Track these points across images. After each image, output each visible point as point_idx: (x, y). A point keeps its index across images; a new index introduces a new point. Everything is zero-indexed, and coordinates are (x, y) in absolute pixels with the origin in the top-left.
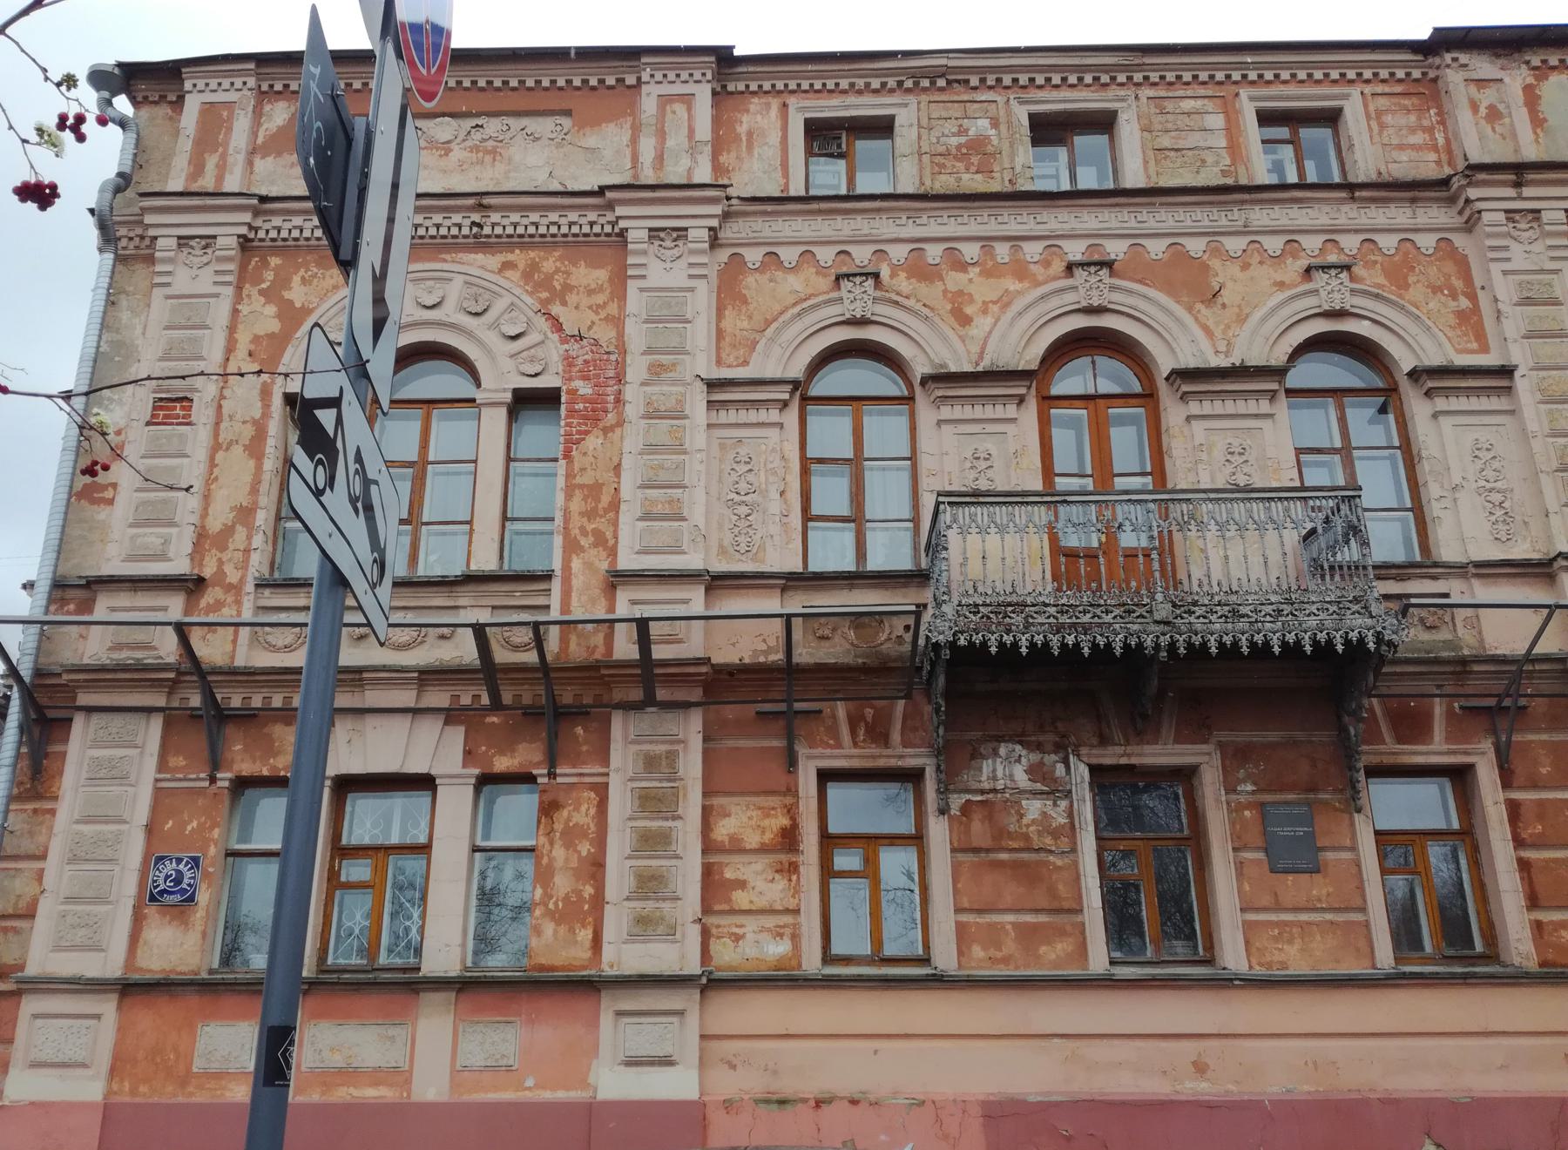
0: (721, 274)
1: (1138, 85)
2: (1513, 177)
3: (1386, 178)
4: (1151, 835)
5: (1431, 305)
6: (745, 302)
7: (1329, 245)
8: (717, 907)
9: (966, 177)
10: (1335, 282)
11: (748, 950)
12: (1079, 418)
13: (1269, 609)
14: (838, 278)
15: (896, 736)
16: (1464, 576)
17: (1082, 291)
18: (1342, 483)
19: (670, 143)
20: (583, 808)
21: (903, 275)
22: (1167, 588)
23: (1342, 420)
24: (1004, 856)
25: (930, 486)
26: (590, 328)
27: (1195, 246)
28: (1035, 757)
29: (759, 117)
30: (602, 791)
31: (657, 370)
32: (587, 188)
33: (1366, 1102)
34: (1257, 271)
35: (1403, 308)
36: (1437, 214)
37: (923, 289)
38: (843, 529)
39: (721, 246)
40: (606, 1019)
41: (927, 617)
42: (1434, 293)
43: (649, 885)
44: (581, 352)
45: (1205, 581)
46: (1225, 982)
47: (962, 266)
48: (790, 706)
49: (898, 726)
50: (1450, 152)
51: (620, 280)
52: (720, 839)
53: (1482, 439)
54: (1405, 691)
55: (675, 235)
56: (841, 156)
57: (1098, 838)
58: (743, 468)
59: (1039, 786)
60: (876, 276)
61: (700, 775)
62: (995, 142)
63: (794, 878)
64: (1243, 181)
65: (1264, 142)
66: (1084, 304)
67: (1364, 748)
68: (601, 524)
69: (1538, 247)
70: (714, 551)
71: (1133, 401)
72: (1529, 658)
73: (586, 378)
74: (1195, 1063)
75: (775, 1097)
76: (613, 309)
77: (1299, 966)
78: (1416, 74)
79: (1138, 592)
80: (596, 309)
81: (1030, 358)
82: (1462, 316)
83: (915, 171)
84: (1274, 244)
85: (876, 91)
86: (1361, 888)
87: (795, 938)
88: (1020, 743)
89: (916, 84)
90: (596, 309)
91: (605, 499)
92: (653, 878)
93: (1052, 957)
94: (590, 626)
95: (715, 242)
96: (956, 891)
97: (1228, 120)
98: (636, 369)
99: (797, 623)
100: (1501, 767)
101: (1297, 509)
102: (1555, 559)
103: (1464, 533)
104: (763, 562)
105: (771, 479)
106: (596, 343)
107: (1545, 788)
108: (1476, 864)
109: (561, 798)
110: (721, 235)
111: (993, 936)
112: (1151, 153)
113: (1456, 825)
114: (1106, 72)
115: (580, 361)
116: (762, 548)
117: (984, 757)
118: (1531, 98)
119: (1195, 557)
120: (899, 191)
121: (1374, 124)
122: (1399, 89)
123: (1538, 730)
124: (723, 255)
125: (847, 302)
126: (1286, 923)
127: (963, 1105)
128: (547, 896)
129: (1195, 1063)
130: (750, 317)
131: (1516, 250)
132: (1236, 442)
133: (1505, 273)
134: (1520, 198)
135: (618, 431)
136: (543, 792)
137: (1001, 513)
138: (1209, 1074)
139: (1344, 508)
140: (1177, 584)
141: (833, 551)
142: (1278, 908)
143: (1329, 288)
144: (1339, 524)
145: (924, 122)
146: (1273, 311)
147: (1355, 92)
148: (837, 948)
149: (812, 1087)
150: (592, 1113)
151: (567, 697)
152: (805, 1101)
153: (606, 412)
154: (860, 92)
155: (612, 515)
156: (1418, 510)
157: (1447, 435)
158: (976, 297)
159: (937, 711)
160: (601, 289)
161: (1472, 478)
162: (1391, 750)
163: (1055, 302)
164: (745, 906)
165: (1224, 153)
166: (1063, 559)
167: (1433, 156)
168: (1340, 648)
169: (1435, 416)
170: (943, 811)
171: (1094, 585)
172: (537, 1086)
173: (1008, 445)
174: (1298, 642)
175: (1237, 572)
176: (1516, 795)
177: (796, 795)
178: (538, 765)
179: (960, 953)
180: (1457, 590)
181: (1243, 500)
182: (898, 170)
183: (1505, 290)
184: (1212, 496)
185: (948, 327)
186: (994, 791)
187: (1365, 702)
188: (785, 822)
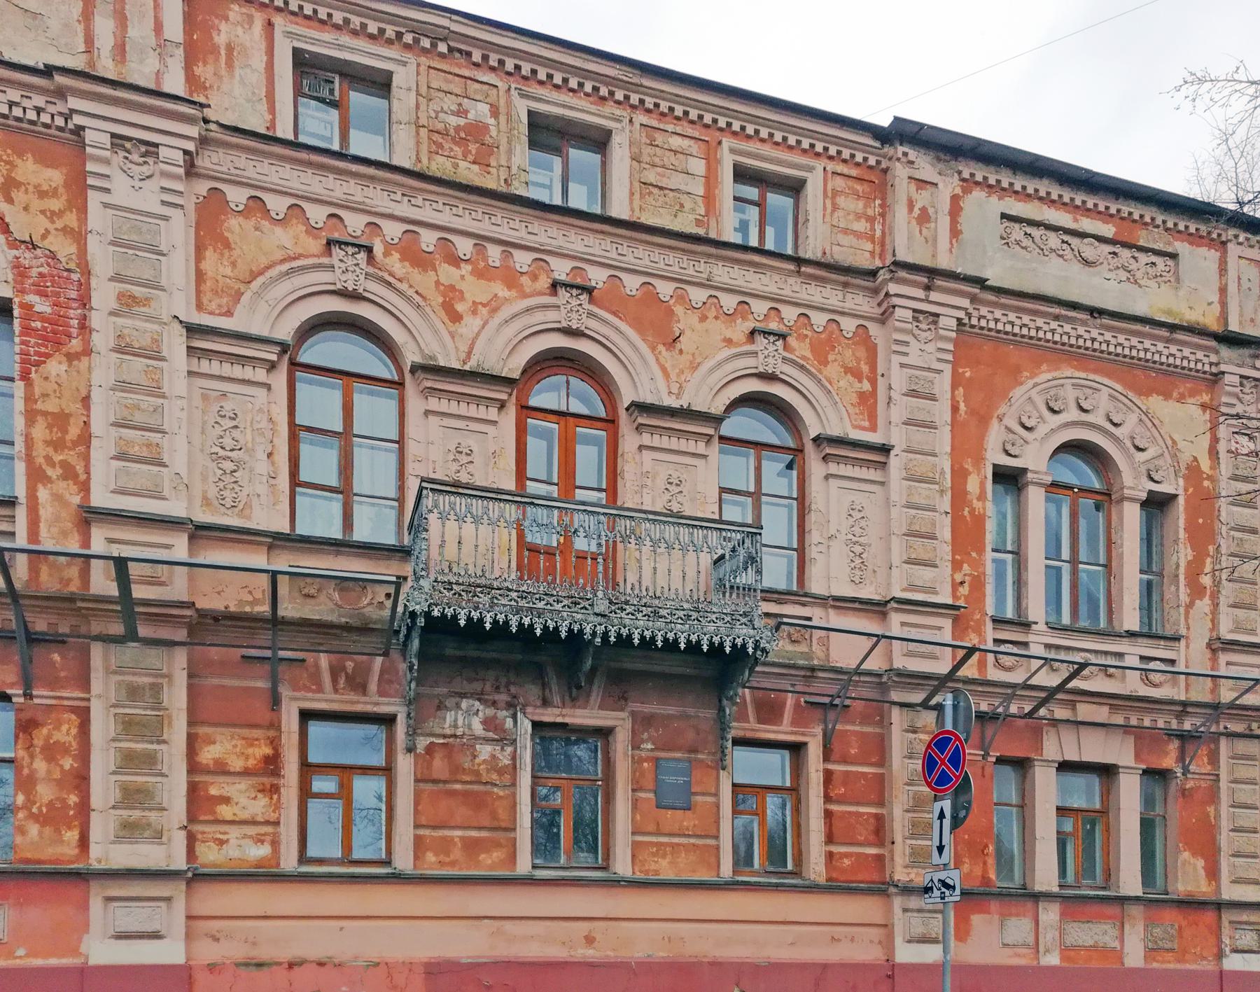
0: (200, 208)
1: (633, 107)
2: (926, 280)
3: (828, 259)
4: (574, 776)
5: (842, 383)
6: (227, 245)
7: (773, 312)
8: (201, 818)
9: (463, 164)
10: (772, 348)
11: (231, 853)
12: (551, 431)
13: (681, 614)
14: (329, 243)
15: (373, 686)
16: (825, 606)
17: (563, 311)
18: (750, 522)
19: (132, 32)
20: (65, 728)
21: (397, 256)
22: (607, 588)
23: (758, 469)
24: (458, 787)
25: (415, 471)
26: (44, 237)
27: (665, 289)
28: (490, 712)
29: (240, 31)
30: (84, 715)
31: (128, 303)
32: (31, 63)
33: (700, 963)
34: (711, 324)
35: (819, 381)
36: (861, 302)
37: (416, 275)
38: (331, 499)
39: (198, 175)
40: (96, 904)
41: (405, 588)
42: (846, 373)
43: (132, 796)
44: (36, 265)
45: (637, 587)
46: (616, 883)
47: (455, 261)
48: (275, 654)
49: (376, 678)
50: (883, 244)
51: (78, 187)
52: (204, 762)
53: (857, 502)
54: (769, 686)
55: (143, 149)
56: (334, 104)
57: (533, 777)
58: (228, 424)
59: (491, 735)
60: (369, 250)
61: (184, 706)
62: (494, 133)
63: (275, 797)
64: (713, 235)
65: (736, 199)
66: (564, 324)
67: (734, 724)
68: (71, 456)
69: (930, 347)
70: (198, 501)
71: (599, 424)
72: (857, 672)
73: (43, 294)
74: (586, 938)
75: (254, 961)
76: (71, 219)
77: (668, 875)
78: (872, 161)
79: (584, 588)
80: (52, 216)
81: (514, 367)
82: (862, 396)
83: (412, 144)
84: (729, 302)
85: (372, 37)
86: (717, 822)
87: (275, 844)
88: (479, 700)
89: (416, 41)
90: (52, 216)
91: (74, 431)
92: (138, 791)
93: (489, 862)
94: (62, 559)
95: (191, 170)
96: (416, 812)
97: (709, 168)
98: (104, 295)
99: (283, 582)
100: (825, 746)
101: (713, 537)
102: (888, 602)
103: (830, 574)
104: (249, 518)
105: (258, 440)
106: (53, 255)
107: (852, 763)
108: (797, 810)
109: (40, 717)
110: (199, 162)
111: (444, 846)
112: (637, 185)
113: (788, 784)
114: (606, 84)
115: (34, 272)
116: (248, 505)
117: (447, 708)
118: (955, 210)
119: (632, 565)
120: (395, 162)
121: (829, 203)
122: (854, 172)
123: (853, 723)
124: (202, 187)
125: (338, 271)
126: (662, 844)
127: (410, 966)
128: (30, 802)
129: (586, 938)
130: (234, 264)
131: (914, 346)
132: (675, 475)
133: (902, 365)
134: (927, 301)
135: (85, 360)
136: (19, 710)
137: (477, 506)
138: (596, 944)
139: (748, 542)
140: (616, 584)
141: (321, 518)
142: (658, 833)
143: (766, 352)
144: (742, 552)
145: (424, 90)
146: (719, 364)
147: (819, 165)
148: (312, 852)
149: (285, 955)
150: (84, 973)
151: (40, 625)
152: (280, 964)
153: (70, 336)
154: (355, 33)
155: (82, 449)
156: (801, 551)
157: (832, 493)
158: (467, 295)
159: (411, 668)
160: (54, 193)
161: (844, 531)
162: (753, 727)
163: (539, 317)
164: (229, 817)
165: (700, 200)
166: (527, 553)
167: (869, 246)
168: (728, 650)
169: (827, 477)
170: (410, 750)
171: (550, 578)
172: (27, 955)
173: (485, 446)
174: (699, 642)
175: (662, 581)
176: (830, 767)
177: (279, 728)
178: (12, 685)
179: (416, 858)
180: (818, 616)
181: (674, 523)
182: (394, 137)
183: (899, 380)
184: (651, 517)
185: (439, 319)
186: (455, 736)
187: (740, 691)
188: (268, 751)
